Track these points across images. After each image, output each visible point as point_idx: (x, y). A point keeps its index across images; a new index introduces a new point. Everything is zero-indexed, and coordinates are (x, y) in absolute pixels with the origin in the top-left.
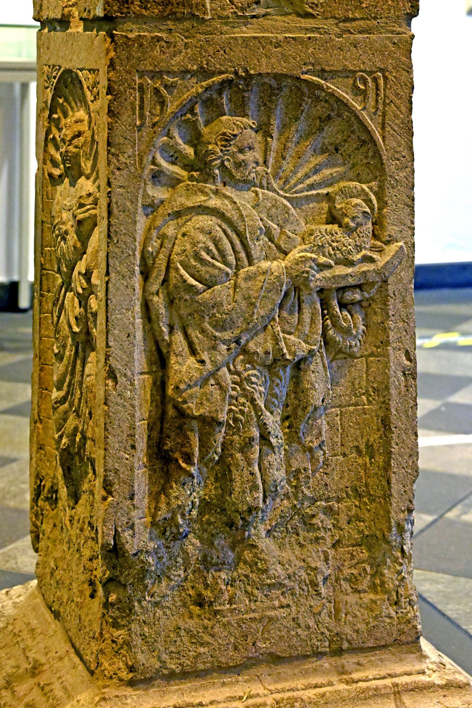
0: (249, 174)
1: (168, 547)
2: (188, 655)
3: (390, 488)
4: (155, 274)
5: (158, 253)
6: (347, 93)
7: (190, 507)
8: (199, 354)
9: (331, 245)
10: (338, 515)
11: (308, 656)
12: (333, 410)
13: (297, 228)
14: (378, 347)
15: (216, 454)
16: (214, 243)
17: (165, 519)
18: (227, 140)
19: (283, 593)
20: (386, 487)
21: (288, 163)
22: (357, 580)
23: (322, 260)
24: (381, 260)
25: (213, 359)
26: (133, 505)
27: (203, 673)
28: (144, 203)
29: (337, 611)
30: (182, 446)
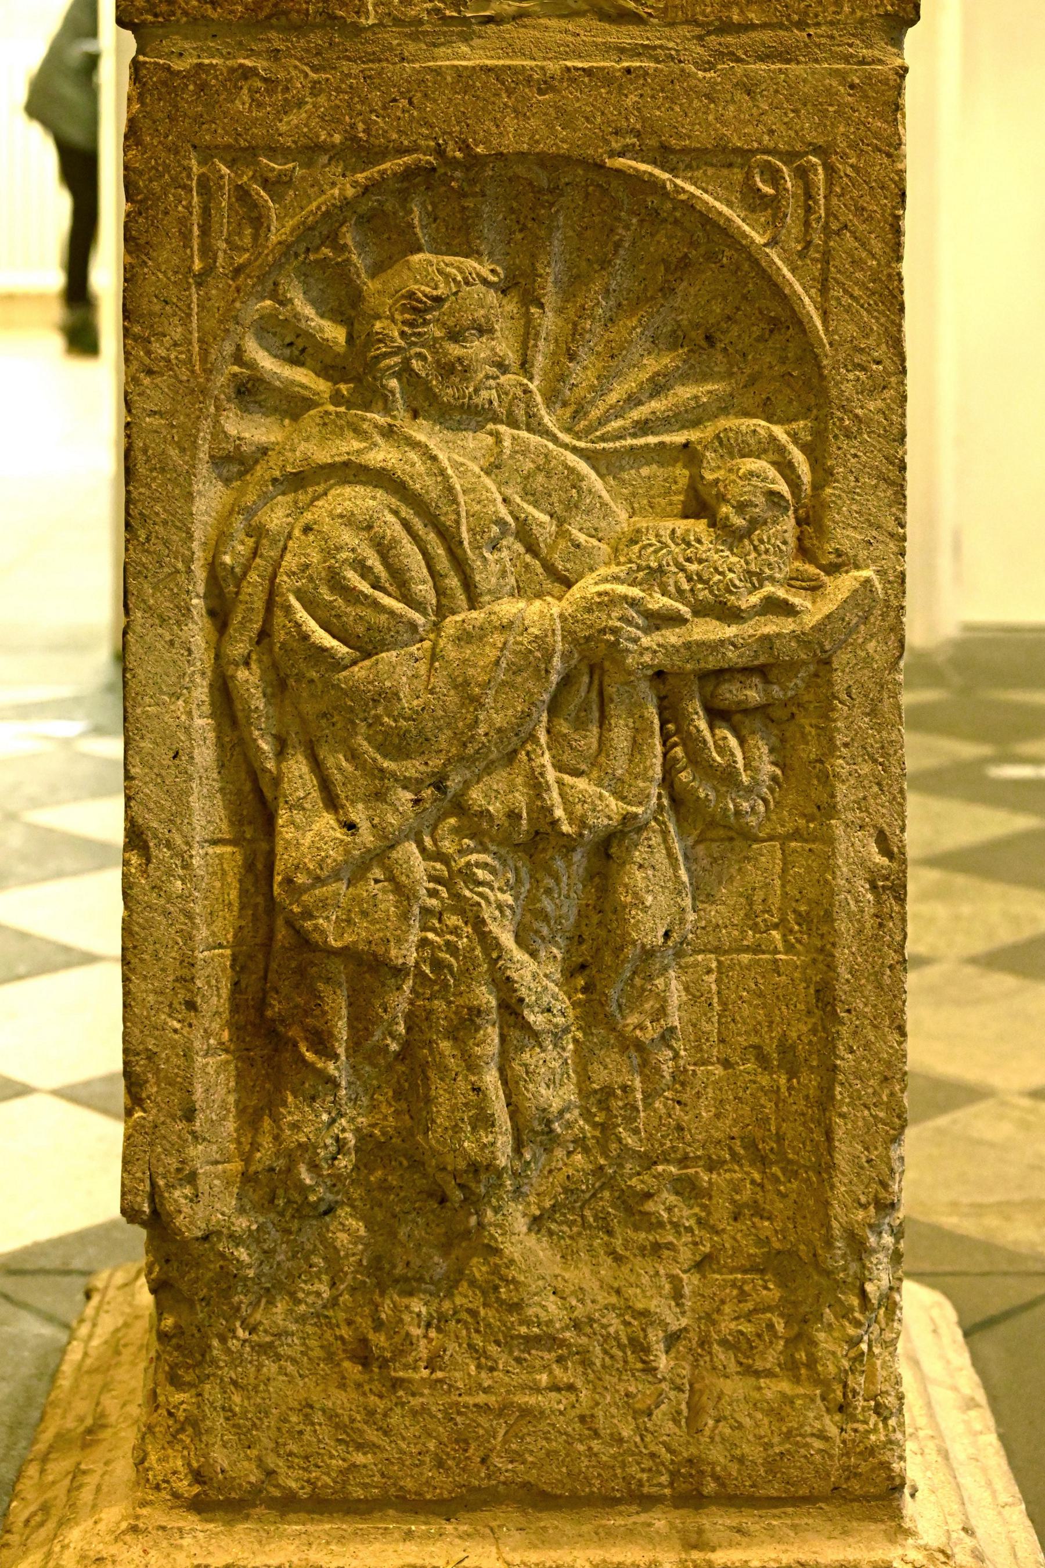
0: (476, 390)
1: (287, 1231)
2: (328, 1466)
3: (831, 1150)
4: (239, 618)
5: (246, 569)
6: (730, 204)
7: (333, 1149)
8: (343, 807)
9: (683, 569)
10: (710, 1198)
11: (617, 1501)
12: (700, 957)
13: (603, 524)
14: (811, 819)
15: (393, 1038)
16: (378, 552)
17: (272, 1169)
18: (415, 309)
19: (560, 1360)
20: (823, 1146)
21: (585, 368)
22: (752, 1348)
23: (658, 601)
24: (814, 611)
25: (376, 821)
26: (193, 1133)
27: (362, 1507)
28: (215, 452)
29: (695, 1410)
30: (307, 1013)
